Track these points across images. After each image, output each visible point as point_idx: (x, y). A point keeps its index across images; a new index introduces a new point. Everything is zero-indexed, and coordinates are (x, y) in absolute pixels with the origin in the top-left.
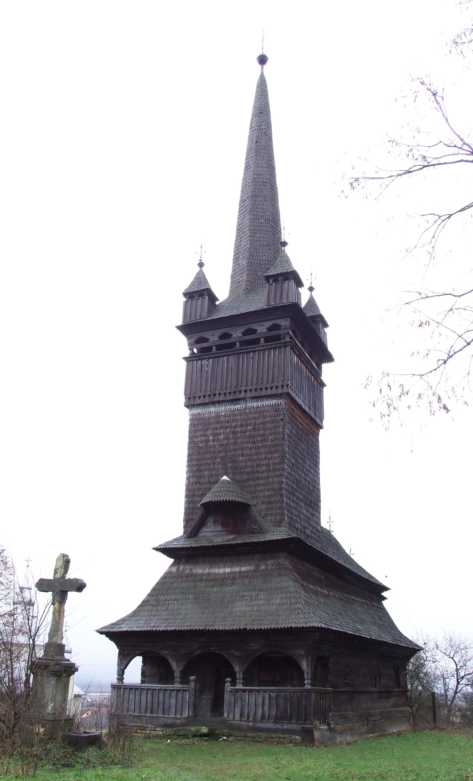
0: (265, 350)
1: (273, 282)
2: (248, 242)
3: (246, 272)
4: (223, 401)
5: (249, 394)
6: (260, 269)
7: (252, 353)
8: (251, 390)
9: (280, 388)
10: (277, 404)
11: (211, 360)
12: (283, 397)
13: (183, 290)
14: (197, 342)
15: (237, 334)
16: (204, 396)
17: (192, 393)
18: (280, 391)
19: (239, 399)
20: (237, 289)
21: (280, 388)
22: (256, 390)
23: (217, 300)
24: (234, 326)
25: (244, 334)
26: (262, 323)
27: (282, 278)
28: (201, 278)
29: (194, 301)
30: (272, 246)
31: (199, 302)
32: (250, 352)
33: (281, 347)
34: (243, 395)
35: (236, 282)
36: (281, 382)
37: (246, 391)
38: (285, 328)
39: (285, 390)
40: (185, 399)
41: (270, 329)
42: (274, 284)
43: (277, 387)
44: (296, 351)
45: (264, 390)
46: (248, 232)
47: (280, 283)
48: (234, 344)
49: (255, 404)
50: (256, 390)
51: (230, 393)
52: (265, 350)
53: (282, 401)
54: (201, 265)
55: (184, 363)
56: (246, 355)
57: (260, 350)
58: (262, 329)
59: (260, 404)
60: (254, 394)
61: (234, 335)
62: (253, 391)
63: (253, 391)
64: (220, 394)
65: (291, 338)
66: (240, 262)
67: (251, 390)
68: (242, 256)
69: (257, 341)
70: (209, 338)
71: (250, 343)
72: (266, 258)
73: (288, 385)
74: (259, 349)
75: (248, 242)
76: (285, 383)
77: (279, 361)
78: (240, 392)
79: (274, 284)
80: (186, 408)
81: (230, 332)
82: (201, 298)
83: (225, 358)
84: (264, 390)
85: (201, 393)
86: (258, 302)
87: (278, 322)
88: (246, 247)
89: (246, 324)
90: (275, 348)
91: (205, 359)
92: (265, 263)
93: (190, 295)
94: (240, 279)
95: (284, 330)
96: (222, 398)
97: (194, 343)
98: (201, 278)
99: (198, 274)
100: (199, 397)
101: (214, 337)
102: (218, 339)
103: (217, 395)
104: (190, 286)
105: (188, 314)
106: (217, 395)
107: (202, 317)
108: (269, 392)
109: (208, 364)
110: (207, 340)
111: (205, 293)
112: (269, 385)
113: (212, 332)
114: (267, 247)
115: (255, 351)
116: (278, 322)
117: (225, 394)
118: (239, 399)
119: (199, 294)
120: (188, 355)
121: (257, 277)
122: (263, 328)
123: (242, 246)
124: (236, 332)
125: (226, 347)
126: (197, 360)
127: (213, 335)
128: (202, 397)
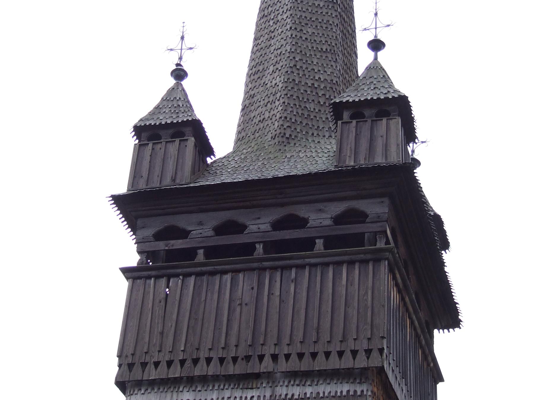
0: (327, 264)
1: (352, 117)
2: (289, 41)
3: (282, 101)
4: (216, 378)
5: (283, 366)
6: (313, 98)
7: (294, 271)
8: (287, 357)
9: (362, 355)
10: (351, 393)
11: (192, 279)
12: (367, 378)
13: (135, 121)
14: (159, 236)
15: (259, 225)
16: (170, 363)
17: (138, 353)
18: (361, 362)
19: (257, 376)
20: (257, 135)
21: (362, 355)
22: (301, 356)
23: (210, 152)
24: (253, 207)
25: (277, 226)
26: (320, 206)
27: (374, 111)
28: (176, 98)
29: (159, 146)
30: (341, 56)
31: (173, 148)
32: (290, 267)
33: (366, 262)
34: (267, 365)
35: (256, 120)
36: (365, 342)
37: (275, 357)
38: (378, 219)
39: (375, 361)
40: (120, 366)
41: (338, 220)
42: (354, 122)
43: (354, 353)
44: (398, 276)
45: (321, 357)
46: (289, 20)
47: (369, 121)
48: (249, 248)
49: (297, 391)
50: (301, 356)
51: (235, 359)
52: (327, 264)
53: (364, 387)
54: (179, 74)
55: (123, 285)
56: (278, 274)
57: (315, 265)
58: (320, 217)
59: (309, 390)
60: (294, 364)
61: (253, 228)
62: (294, 357)
63: (294, 357)
64: (209, 360)
65: (387, 242)
66: (266, 80)
67: (287, 357)
68: (272, 68)
69: (308, 244)
70: (190, 229)
71: (289, 249)
72: (327, 78)
73: (381, 351)
74: (313, 261)
75: (289, 41)
76: (376, 344)
77: (362, 292)
78: (261, 358)
79: (354, 122)
80: (117, 390)
81: (241, 219)
82: (177, 140)
83: (228, 277)
84: (321, 357)
85: (161, 354)
86: (316, 156)
87: (363, 205)
88: (283, 50)
89: (282, 205)
90: (351, 263)
91: (177, 276)
92: (325, 87)
93: (147, 133)
94: (267, 115)
95: (374, 225)
96: (213, 369)
97: (152, 239)
98: (176, 98)
99: (172, 91)
100: (157, 364)
101: (201, 229)
102: (211, 233)
103: (203, 362)
104: (152, 114)
105: (145, 174)
106: (203, 362)
107: (178, 181)
108: (334, 363)
109: (178, 290)
110: (184, 234)
111: (188, 130)
112: (335, 348)
113: (202, 216)
114: (329, 55)
115: (303, 267)
116: (363, 205)
117: (222, 360)
118: (257, 376)
119: (168, 131)
120: (135, 264)
121: (306, 114)
122: (324, 215)
123: (272, 49)
124: (258, 221)
125: (230, 253)
126: (157, 277)
127: (200, 223)
128: (163, 365)
